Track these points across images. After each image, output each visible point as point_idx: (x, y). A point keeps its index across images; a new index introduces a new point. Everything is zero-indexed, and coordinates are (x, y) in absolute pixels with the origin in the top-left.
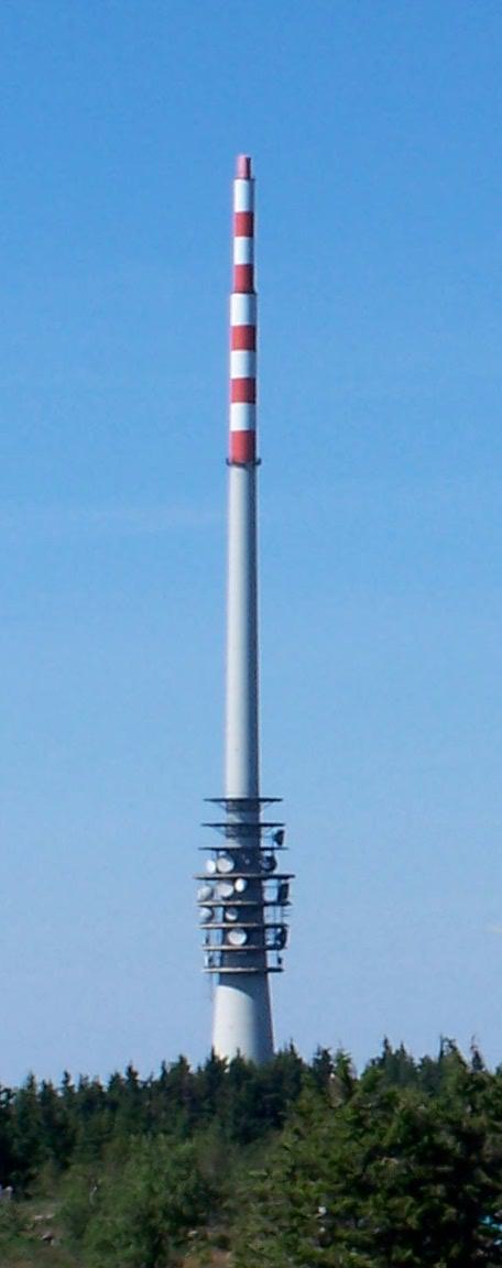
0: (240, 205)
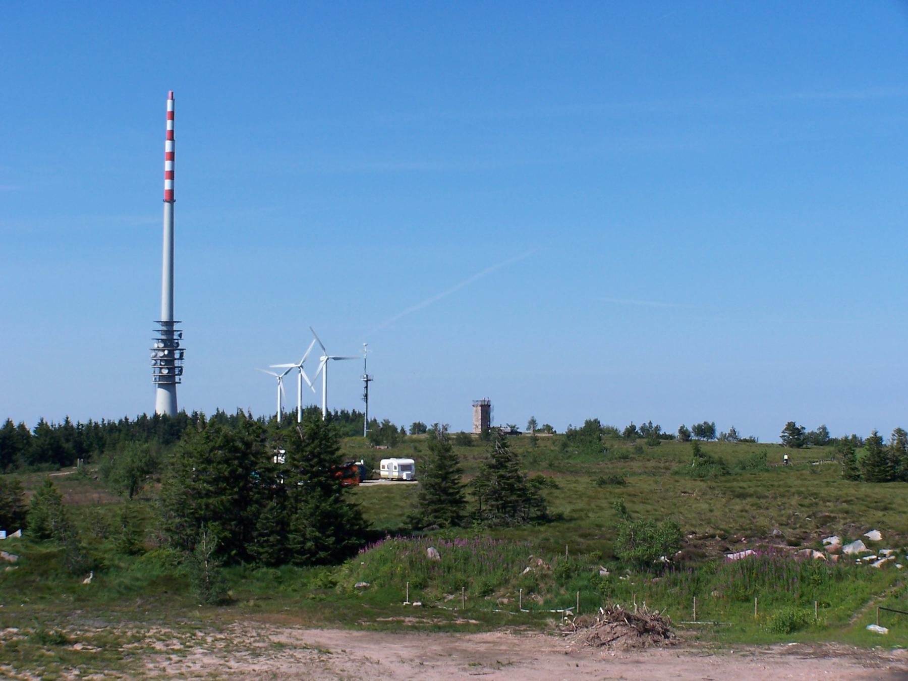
0: (169, 109)
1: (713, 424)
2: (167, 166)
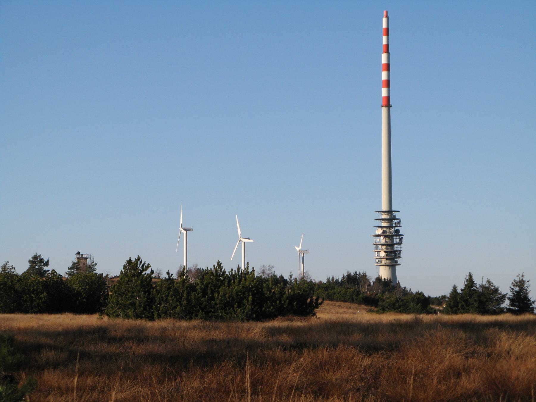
0: (384, 26)
1: (488, 282)
2: (384, 76)
